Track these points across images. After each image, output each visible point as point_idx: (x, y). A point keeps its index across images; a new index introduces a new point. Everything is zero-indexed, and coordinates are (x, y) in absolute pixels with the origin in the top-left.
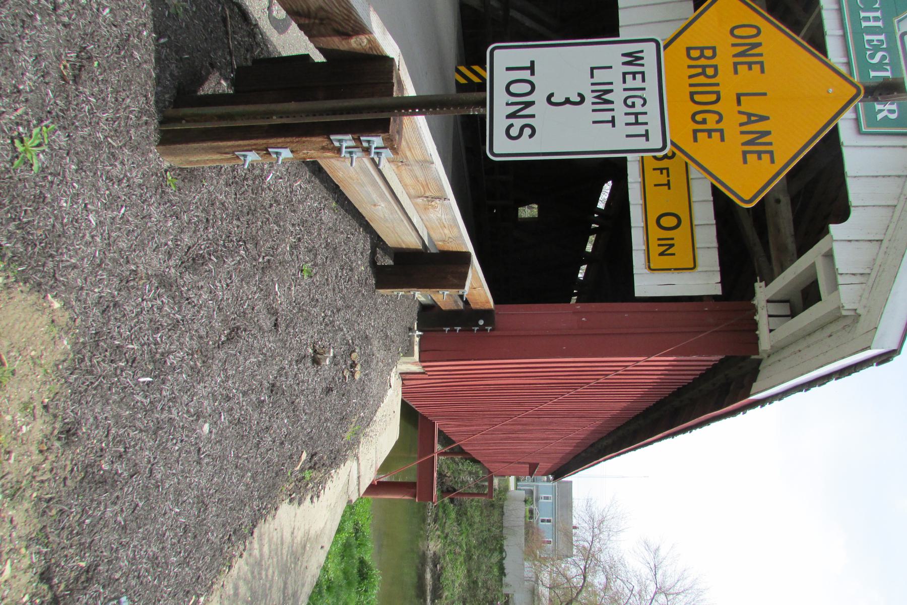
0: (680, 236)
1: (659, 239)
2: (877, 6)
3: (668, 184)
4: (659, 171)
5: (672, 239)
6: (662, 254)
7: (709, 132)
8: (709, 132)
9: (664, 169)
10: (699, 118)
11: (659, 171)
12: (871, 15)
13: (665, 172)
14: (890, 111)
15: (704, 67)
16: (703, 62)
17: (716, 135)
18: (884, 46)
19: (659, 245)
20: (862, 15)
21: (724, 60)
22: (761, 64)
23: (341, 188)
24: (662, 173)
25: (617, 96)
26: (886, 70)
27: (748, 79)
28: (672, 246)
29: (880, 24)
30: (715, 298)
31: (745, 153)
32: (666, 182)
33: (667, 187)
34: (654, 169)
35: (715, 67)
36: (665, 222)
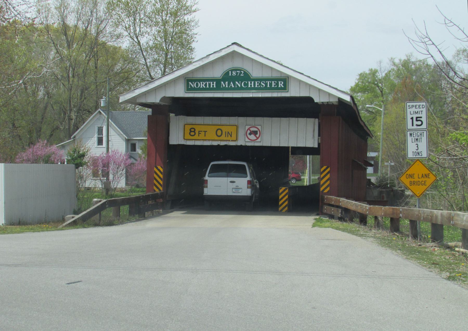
0: (225, 129)
2: (247, 82)
3: (205, 132)
4: (200, 134)
5: (226, 132)
6: (231, 136)
7: (425, 183)
8: (425, 183)
9: (199, 132)
10: (422, 184)
11: (200, 134)
12: (249, 84)
13: (200, 132)
14: (281, 83)
15: (414, 183)
16: (412, 183)
17: (425, 182)
18: (259, 82)
19: (228, 137)
20: (249, 86)
21: (412, 180)
22: (413, 174)
23: (324, 228)
24: (201, 133)
26: (267, 82)
27: (416, 176)
28: (228, 133)
31: (428, 178)
32: (204, 132)
33: (206, 132)
34: (199, 136)
35: (413, 181)
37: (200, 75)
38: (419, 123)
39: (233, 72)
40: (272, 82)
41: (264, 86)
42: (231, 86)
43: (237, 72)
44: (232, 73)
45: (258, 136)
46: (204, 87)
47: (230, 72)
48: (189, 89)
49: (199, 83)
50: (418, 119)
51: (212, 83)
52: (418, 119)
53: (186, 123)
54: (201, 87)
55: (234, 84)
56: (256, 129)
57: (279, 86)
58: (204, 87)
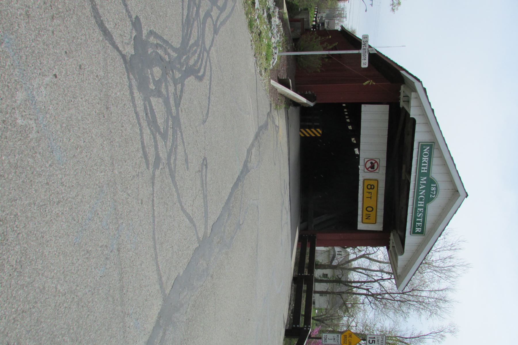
1: (366, 214)
2: (423, 200)
3: (371, 198)
6: (367, 219)
13: (370, 193)
14: (419, 230)
20: (419, 202)
21: (348, 336)
25: (336, 339)
26: (421, 219)
27: (350, 338)
28: (369, 216)
29: (423, 205)
30: (380, 231)
33: (370, 198)
34: (367, 192)
36: (368, 209)
37: (435, 153)
38: (371, 342)
39: (435, 188)
40: (421, 223)
41: (418, 216)
42: (421, 186)
43: (435, 192)
44: (433, 187)
45: (370, 169)
46: (423, 161)
47: (435, 185)
48: (422, 146)
49: (428, 156)
50: (374, 341)
51: (426, 168)
52: (374, 341)
53: (379, 181)
54: (423, 158)
55: (423, 189)
56: (375, 168)
57: (416, 229)
58: (423, 161)
